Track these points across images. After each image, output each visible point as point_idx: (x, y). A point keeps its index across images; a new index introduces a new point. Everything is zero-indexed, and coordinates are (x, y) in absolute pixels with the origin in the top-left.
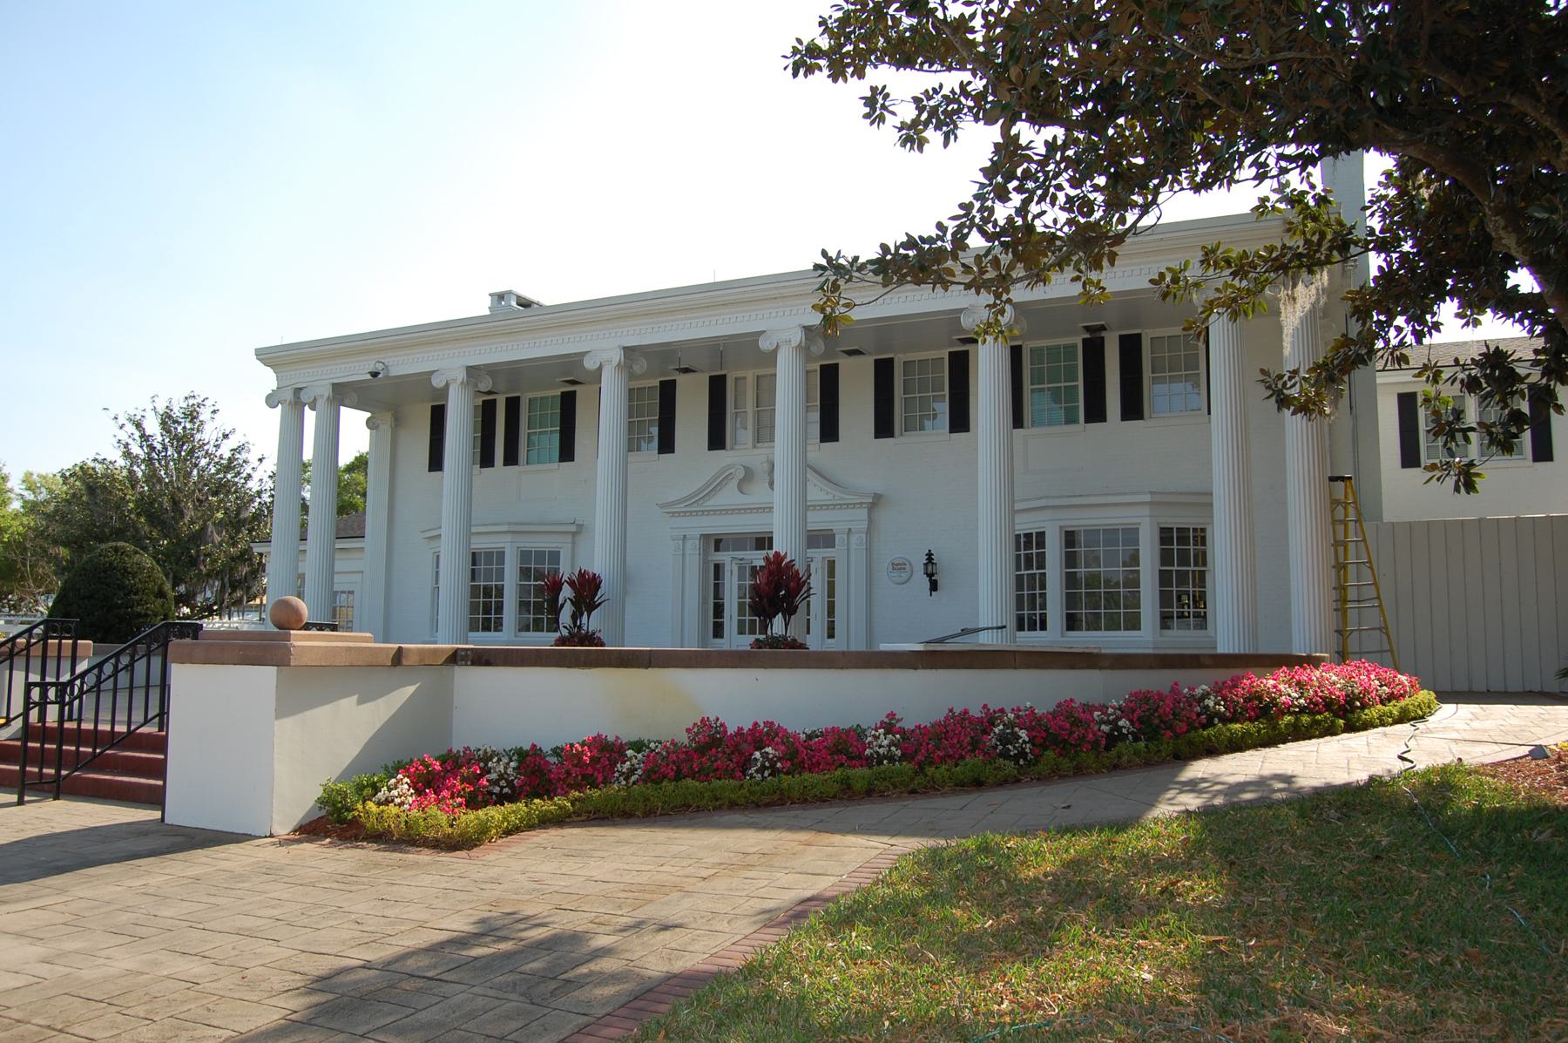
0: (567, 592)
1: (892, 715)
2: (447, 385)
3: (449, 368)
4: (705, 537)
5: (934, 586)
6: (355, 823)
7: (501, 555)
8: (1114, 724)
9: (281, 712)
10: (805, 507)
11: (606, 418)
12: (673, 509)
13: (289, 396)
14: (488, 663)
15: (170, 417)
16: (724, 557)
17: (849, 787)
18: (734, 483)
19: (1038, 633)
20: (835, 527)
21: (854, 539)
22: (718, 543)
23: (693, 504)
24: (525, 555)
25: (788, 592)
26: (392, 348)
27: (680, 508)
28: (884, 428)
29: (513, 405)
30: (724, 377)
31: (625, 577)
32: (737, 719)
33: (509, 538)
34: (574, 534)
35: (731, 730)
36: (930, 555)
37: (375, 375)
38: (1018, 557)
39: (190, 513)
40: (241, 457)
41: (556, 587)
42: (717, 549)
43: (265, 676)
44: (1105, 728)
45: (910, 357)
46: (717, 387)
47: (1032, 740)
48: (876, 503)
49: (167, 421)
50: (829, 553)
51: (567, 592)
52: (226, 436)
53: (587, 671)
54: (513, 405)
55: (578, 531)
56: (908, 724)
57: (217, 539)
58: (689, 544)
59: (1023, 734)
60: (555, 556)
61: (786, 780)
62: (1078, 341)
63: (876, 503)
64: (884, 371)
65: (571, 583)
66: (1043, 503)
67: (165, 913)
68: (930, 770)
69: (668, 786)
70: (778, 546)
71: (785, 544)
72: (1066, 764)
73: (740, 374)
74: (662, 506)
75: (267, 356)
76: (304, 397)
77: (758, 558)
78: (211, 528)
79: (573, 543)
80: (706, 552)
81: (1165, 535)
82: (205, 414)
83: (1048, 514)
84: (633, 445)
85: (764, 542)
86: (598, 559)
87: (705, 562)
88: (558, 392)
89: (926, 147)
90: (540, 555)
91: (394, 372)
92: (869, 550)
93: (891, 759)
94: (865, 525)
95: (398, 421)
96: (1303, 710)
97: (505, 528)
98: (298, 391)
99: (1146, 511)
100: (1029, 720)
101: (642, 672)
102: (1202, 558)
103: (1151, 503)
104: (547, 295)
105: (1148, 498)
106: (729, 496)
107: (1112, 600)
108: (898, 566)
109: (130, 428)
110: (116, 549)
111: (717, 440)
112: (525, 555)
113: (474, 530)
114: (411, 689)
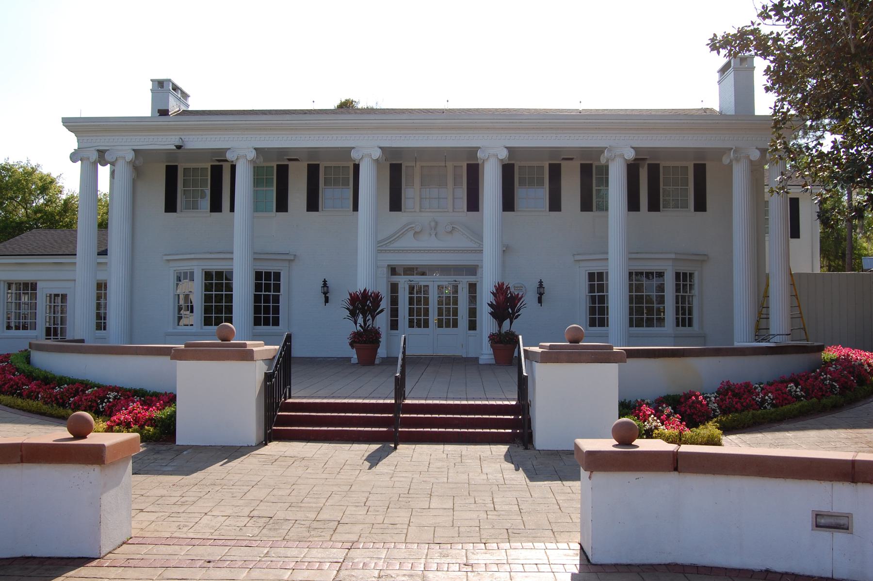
5: (327, 300)
19: (103, 331)
22: (393, 271)
26: (377, 128)
28: (313, 205)
29: (654, 170)
36: (325, 281)
37: (179, 147)
45: (523, 164)
50: (472, 279)
53: (648, 360)
54: (654, 170)
62: (208, 166)
64: (313, 172)
67: (205, 527)
75: (71, 124)
81: (678, 275)
83: (195, 263)
89: (712, 36)
98: (101, 153)
102: (229, 288)
104: (363, 103)
105: (673, 256)
106: (408, 242)
107: (650, 310)
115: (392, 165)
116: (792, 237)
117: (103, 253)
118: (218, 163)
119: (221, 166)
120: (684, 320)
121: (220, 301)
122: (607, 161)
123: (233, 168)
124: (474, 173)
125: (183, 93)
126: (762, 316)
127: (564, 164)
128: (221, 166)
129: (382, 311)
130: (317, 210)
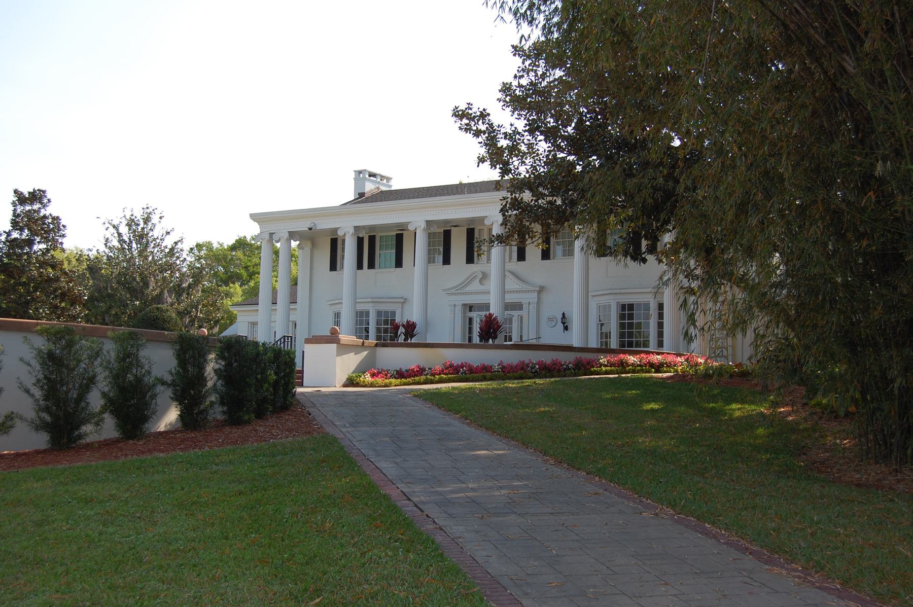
0: (402, 330)
3: (346, 229)
4: (464, 305)
5: (566, 328)
7: (368, 313)
10: (503, 292)
11: (418, 249)
12: (449, 292)
13: (267, 237)
15: (133, 220)
16: (474, 314)
18: (477, 281)
20: (523, 301)
21: (531, 306)
22: (471, 308)
23: (460, 289)
27: (453, 291)
29: (372, 239)
30: (473, 229)
31: (427, 323)
33: (371, 305)
34: (403, 303)
36: (564, 314)
37: (310, 229)
39: (152, 284)
40: (179, 246)
41: (397, 327)
42: (470, 311)
43: (334, 346)
46: (470, 233)
48: (541, 290)
49: (131, 223)
50: (520, 313)
51: (402, 330)
52: (168, 233)
54: (372, 239)
55: (404, 301)
57: (169, 300)
58: (457, 308)
60: (393, 313)
63: (541, 290)
65: (403, 326)
73: (481, 228)
74: (444, 290)
75: (255, 217)
76: (275, 237)
77: (483, 313)
78: (166, 294)
80: (464, 313)
82: (155, 219)
83: (612, 297)
84: (430, 260)
85: (487, 307)
86: (414, 314)
87: (464, 317)
88: (394, 233)
90: (386, 313)
91: (319, 227)
92: (538, 311)
94: (536, 300)
95: (314, 245)
96: (638, 365)
98: (271, 234)
100: (540, 363)
101: (465, 181)
106: (475, 286)
108: (550, 319)
109: (112, 230)
110: (158, 309)
111: (470, 260)
112: (379, 313)
114: (366, 353)
115: (358, 238)
117: (275, 303)
120: (606, 337)
121: (637, 342)
123: (344, 241)
124: (335, 244)
125: (382, 177)
127: (453, 229)
130: (335, 270)
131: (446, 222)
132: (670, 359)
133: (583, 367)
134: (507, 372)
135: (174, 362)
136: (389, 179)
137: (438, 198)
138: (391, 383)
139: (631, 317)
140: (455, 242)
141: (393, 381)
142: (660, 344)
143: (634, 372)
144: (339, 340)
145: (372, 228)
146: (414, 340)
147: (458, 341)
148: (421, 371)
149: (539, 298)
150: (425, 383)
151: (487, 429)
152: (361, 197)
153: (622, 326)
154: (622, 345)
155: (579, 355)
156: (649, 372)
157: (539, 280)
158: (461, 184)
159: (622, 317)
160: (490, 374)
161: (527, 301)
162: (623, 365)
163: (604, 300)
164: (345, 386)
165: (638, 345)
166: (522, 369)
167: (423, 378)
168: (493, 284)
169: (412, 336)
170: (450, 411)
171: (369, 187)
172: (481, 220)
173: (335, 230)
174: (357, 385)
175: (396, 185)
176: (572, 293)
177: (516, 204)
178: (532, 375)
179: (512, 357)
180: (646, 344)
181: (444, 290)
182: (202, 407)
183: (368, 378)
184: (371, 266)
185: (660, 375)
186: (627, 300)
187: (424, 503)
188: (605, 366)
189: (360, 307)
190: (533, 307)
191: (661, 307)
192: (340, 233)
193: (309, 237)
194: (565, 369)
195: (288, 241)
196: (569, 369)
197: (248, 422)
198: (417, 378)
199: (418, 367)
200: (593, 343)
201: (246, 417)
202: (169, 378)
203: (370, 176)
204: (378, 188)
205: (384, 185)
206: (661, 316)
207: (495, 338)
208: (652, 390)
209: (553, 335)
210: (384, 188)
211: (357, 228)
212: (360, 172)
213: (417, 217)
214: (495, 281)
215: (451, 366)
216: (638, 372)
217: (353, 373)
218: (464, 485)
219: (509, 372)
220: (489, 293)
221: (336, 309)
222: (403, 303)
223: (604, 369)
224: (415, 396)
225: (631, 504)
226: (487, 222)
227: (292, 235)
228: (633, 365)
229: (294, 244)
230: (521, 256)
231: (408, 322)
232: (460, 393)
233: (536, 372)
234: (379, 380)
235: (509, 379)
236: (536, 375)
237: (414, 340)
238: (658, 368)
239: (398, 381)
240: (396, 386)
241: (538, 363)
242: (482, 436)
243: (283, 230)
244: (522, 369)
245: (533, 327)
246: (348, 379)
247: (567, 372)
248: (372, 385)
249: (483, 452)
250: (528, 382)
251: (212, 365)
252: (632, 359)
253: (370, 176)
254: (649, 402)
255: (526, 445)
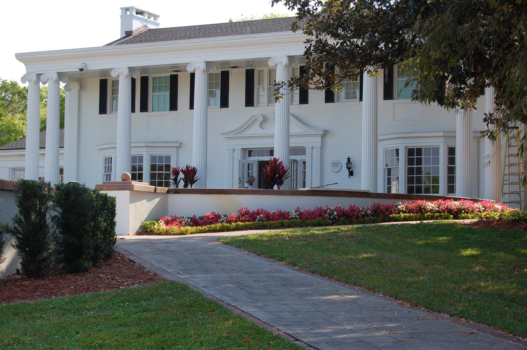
0: (181, 175)
1: (298, 208)
2: (118, 76)
3: (120, 68)
4: (244, 150)
5: (351, 174)
6: (152, 231)
7: (141, 158)
8: (366, 212)
9: (131, 203)
10: (288, 136)
12: (229, 136)
14: (179, 193)
17: (283, 225)
18: (257, 124)
21: (315, 151)
22: (251, 153)
23: (238, 133)
24: (153, 158)
25: (279, 175)
27: (232, 135)
29: (145, 81)
30: (253, 70)
32: (252, 209)
33: (145, 149)
34: (178, 148)
35: (251, 211)
36: (349, 159)
37: (81, 70)
38: (105, 167)
42: (250, 155)
43: (127, 193)
44: (363, 213)
46: (250, 75)
47: (337, 214)
48: (325, 134)
51: (181, 175)
53: (208, 195)
54: (145, 81)
56: (302, 211)
58: (236, 153)
59: (335, 213)
60: (168, 158)
61: (265, 223)
62: (219, 71)
63: (325, 134)
65: (183, 171)
66: (397, 136)
68: (306, 221)
69: (233, 224)
70: (276, 155)
71: (279, 155)
72: (347, 221)
73: (261, 69)
75: (21, 57)
79: (177, 152)
80: (244, 158)
88: (169, 75)
90: (161, 158)
92: (322, 157)
93: (296, 218)
95: (82, 86)
96: (437, 212)
97: (144, 145)
98: (39, 75)
99: (442, 140)
100: (337, 209)
103: (444, 136)
105: (442, 134)
106: (255, 130)
108: (335, 164)
111: (250, 102)
112: (153, 158)
113: (132, 145)
114: (158, 200)
116: (132, 112)
117: (43, 148)
118: (176, 73)
119: (177, 75)
122: (118, 76)
125: (150, 15)
126: (505, 182)
128: (177, 75)
129: (179, 181)
131: (224, 63)
132: (468, 204)
133: (381, 214)
134: (305, 219)
135: (15, 210)
136: (156, 17)
137: (218, 38)
138: (187, 231)
139: (419, 162)
140: (236, 83)
141: (189, 228)
142: (451, 189)
143: (432, 218)
144: (132, 186)
145: (144, 69)
146: (194, 186)
147: (236, 187)
148: (216, 218)
149: (323, 143)
150: (222, 230)
151: (321, 275)
152: (128, 37)
153: (410, 171)
154: (410, 190)
155: (377, 201)
156: (447, 218)
157: (323, 124)
158: (231, 23)
159: (410, 162)
160: (287, 221)
161: (310, 145)
162: (421, 212)
163: (393, 145)
164: (138, 233)
165: (427, 190)
166: (320, 215)
167: (219, 225)
168: (276, 128)
169: (193, 182)
170: (272, 257)
171: (137, 26)
172: (264, 61)
173: (107, 72)
174: (151, 233)
175: (164, 23)
176: (361, 136)
177: (321, 46)
178: (330, 222)
179: (309, 204)
180: (436, 189)
181: (222, 134)
182: (45, 255)
183: (163, 226)
184: (144, 108)
185: (456, 221)
186: (415, 144)
187: (313, 342)
188: (404, 212)
189: (135, 152)
190: (316, 153)
191: (452, 151)
192: (114, 74)
193: (78, 79)
194: (363, 216)
195: (57, 82)
196: (368, 216)
197: (86, 270)
198: (213, 226)
199: (213, 213)
200: (381, 189)
201: (86, 265)
202: (12, 225)
203: (137, 13)
204: (146, 26)
205: (151, 23)
206: (452, 160)
207: (280, 183)
208: (464, 236)
209: (345, 183)
210: (151, 27)
211: (131, 69)
212: (127, 9)
213: (195, 58)
214: (276, 126)
215: (247, 213)
216: (436, 218)
217: (146, 220)
218: (341, 327)
219: (307, 219)
220: (273, 136)
221: (108, 153)
222: (178, 148)
223: (402, 215)
224: (227, 243)
225: (511, 342)
226: (271, 64)
227: (61, 76)
228: (431, 211)
229: (62, 85)
230: (304, 99)
231: (187, 168)
232: (269, 241)
233: (334, 218)
234: (175, 228)
235: (467, 224)
236: (335, 222)
237: (194, 186)
238: (457, 214)
239: (194, 229)
240: (195, 235)
241: (336, 209)
242: (325, 283)
243: (51, 71)
244: (320, 215)
245: (322, 173)
246: (141, 227)
247: (367, 218)
248: (167, 233)
249: (335, 297)
250: (333, 229)
251: (52, 212)
252: (430, 205)
253: (137, 13)
254: (466, 248)
255: (373, 290)
